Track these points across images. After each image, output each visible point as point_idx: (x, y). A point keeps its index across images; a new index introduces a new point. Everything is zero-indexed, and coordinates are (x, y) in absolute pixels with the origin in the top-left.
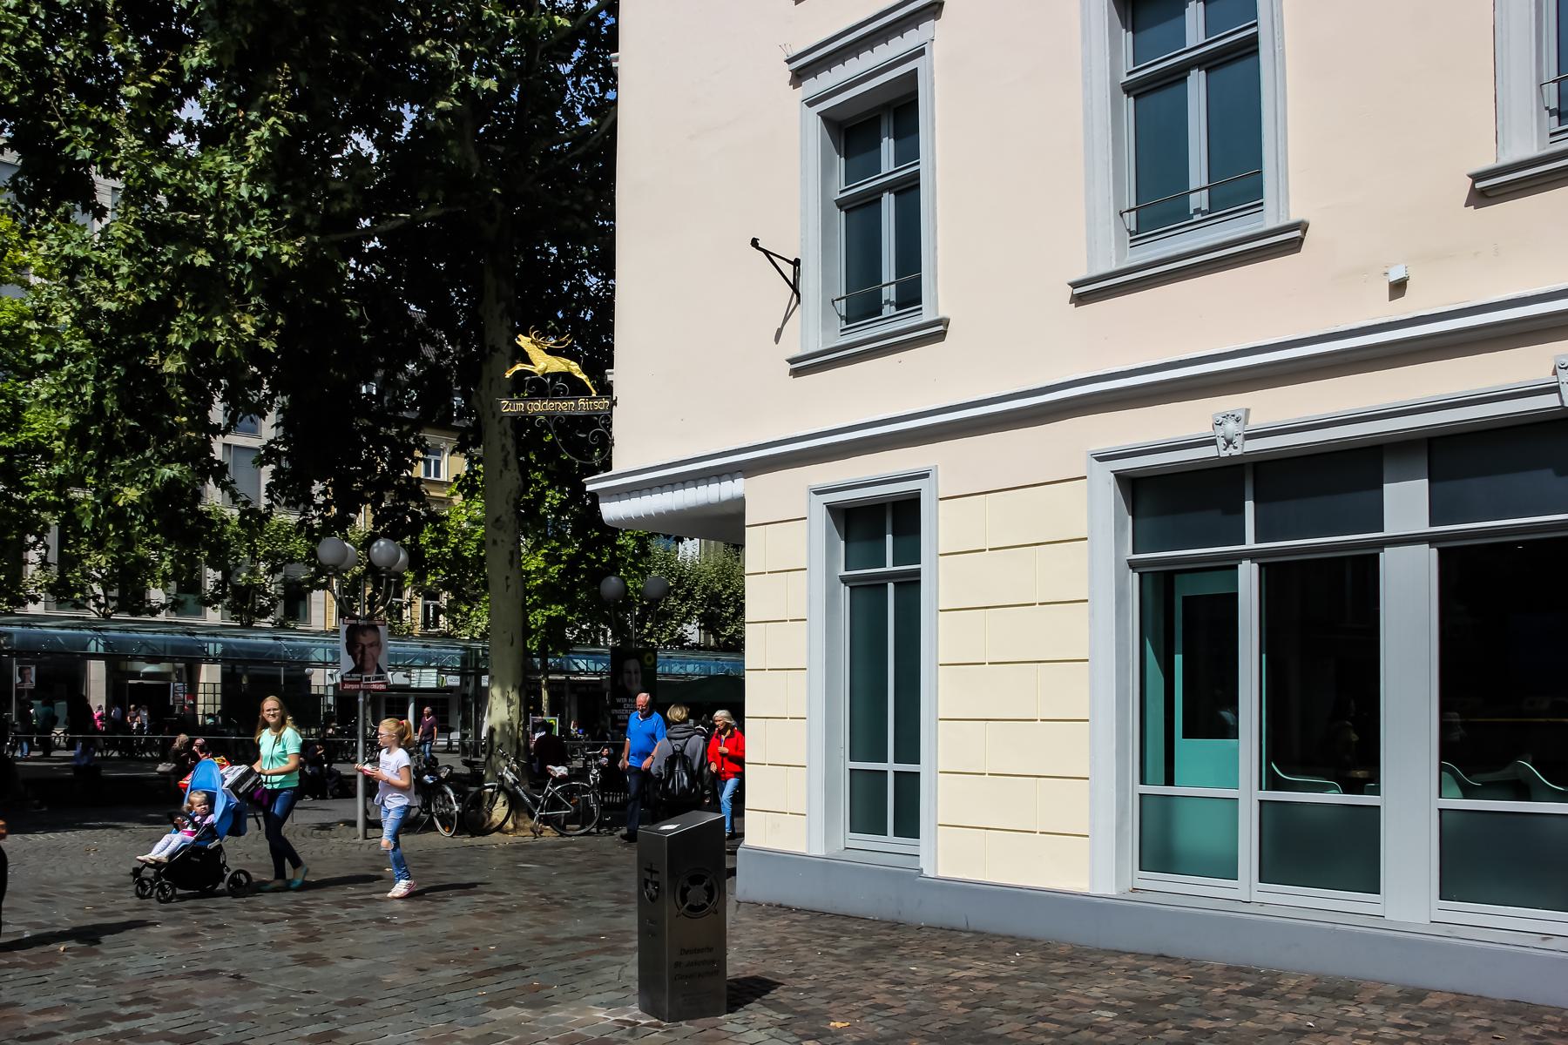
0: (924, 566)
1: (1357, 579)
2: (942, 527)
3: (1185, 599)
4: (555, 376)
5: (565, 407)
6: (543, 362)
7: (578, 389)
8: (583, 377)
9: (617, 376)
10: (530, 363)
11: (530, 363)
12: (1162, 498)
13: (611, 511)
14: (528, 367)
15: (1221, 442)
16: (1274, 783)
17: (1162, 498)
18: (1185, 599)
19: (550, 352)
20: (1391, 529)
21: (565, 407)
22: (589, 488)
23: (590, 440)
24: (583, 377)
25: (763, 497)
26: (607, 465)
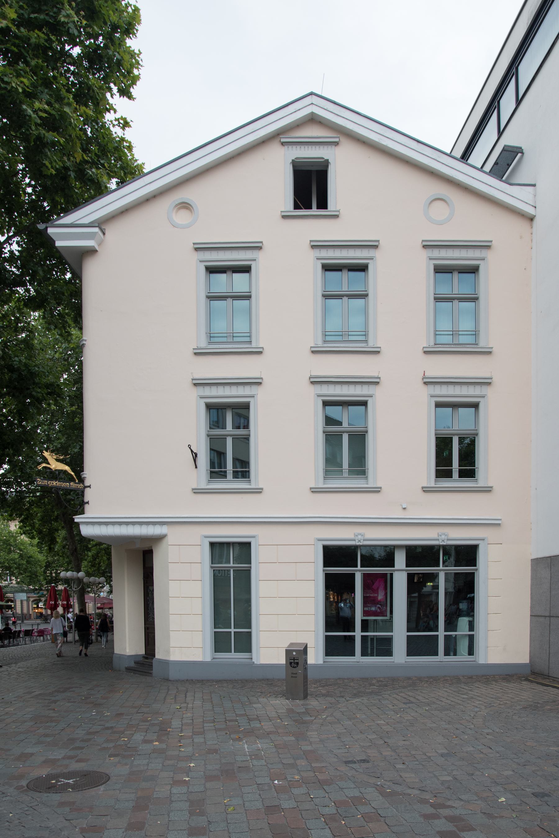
0: (253, 565)
1: (387, 581)
2: (259, 555)
3: (406, 567)
4: (61, 471)
5: (66, 485)
6: (55, 465)
7: (71, 479)
8: (73, 473)
9: (90, 472)
10: (49, 464)
11: (49, 464)
12: (334, 555)
13: (85, 531)
14: (48, 466)
15: (357, 541)
16: (326, 631)
17: (334, 555)
18: (406, 567)
19: (58, 460)
20: (397, 567)
21: (66, 485)
22: (76, 520)
23: (74, 502)
24: (73, 473)
25: (174, 536)
26: (83, 513)
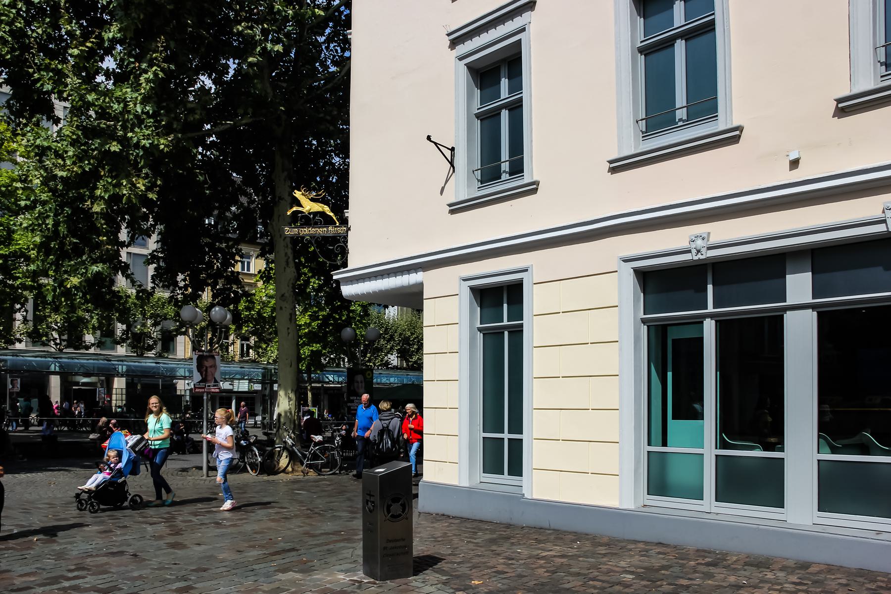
0: (525, 322)
1: (771, 329)
2: (535, 300)
3: (674, 341)
4: (315, 214)
5: (321, 231)
6: (308, 206)
7: (328, 221)
8: (331, 214)
9: (351, 214)
10: (301, 206)
11: (301, 206)
12: (660, 283)
13: (347, 290)
14: (300, 209)
15: (694, 251)
16: (724, 445)
17: (660, 283)
18: (674, 341)
19: (312, 200)
20: (790, 301)
21: (321, 231)
22: (335, 277)
23: (335, 250)
24: (331, 214)
25: (433, 282)
26: (345, 264)
